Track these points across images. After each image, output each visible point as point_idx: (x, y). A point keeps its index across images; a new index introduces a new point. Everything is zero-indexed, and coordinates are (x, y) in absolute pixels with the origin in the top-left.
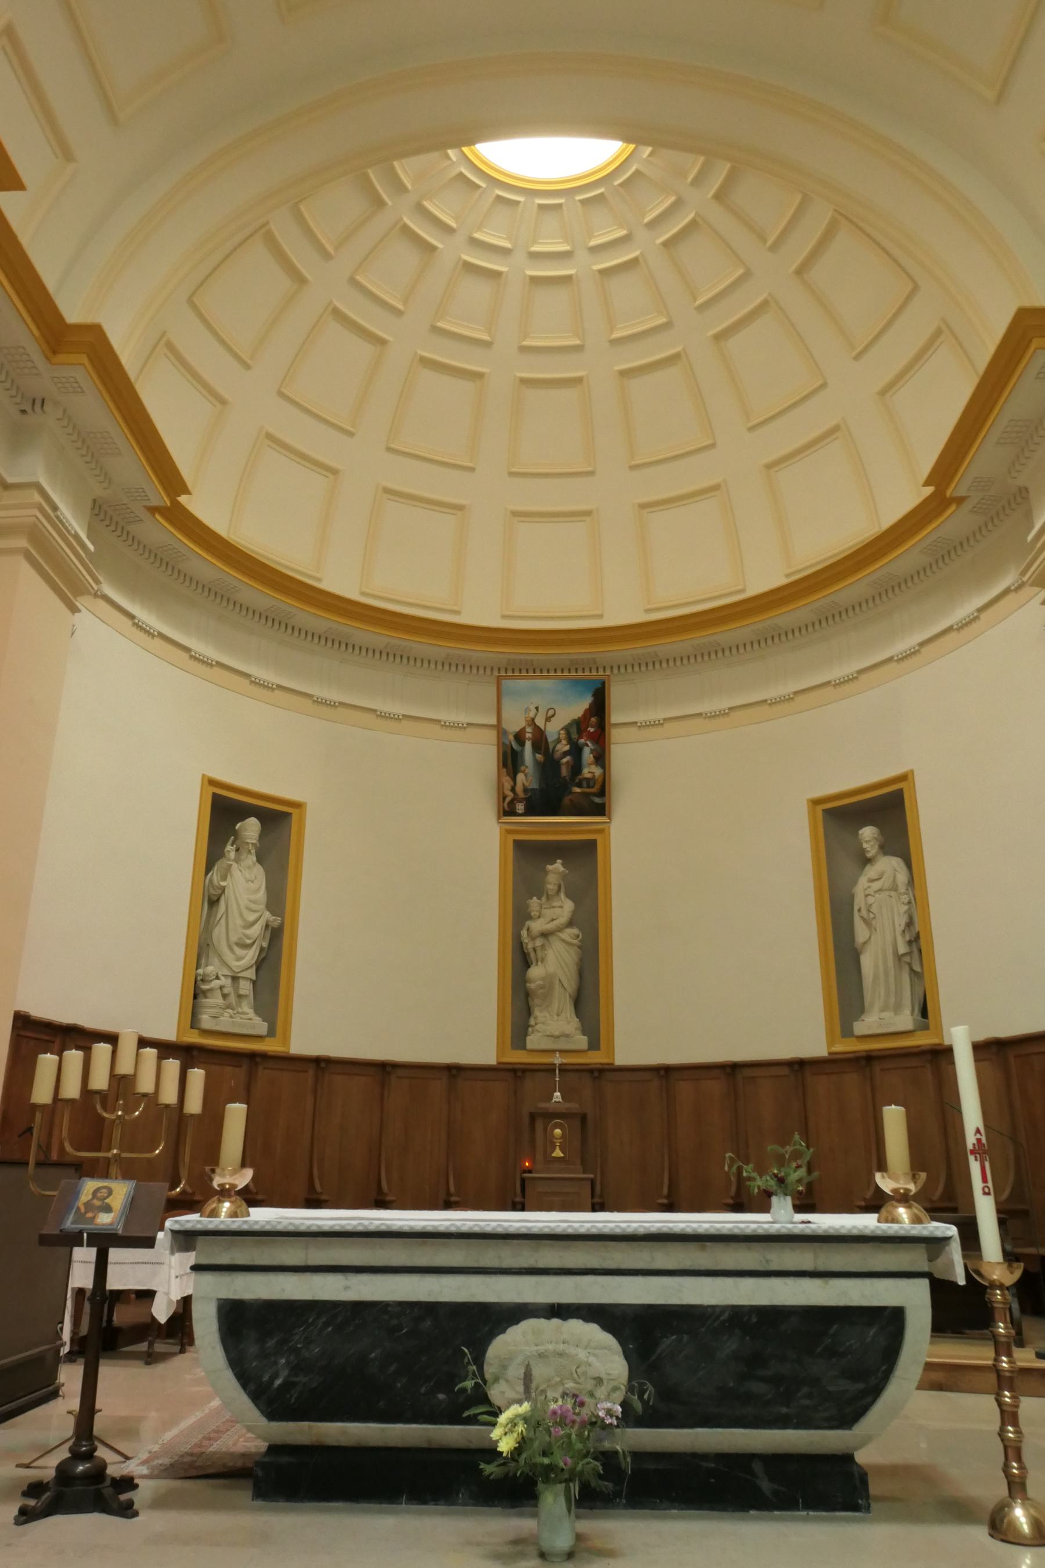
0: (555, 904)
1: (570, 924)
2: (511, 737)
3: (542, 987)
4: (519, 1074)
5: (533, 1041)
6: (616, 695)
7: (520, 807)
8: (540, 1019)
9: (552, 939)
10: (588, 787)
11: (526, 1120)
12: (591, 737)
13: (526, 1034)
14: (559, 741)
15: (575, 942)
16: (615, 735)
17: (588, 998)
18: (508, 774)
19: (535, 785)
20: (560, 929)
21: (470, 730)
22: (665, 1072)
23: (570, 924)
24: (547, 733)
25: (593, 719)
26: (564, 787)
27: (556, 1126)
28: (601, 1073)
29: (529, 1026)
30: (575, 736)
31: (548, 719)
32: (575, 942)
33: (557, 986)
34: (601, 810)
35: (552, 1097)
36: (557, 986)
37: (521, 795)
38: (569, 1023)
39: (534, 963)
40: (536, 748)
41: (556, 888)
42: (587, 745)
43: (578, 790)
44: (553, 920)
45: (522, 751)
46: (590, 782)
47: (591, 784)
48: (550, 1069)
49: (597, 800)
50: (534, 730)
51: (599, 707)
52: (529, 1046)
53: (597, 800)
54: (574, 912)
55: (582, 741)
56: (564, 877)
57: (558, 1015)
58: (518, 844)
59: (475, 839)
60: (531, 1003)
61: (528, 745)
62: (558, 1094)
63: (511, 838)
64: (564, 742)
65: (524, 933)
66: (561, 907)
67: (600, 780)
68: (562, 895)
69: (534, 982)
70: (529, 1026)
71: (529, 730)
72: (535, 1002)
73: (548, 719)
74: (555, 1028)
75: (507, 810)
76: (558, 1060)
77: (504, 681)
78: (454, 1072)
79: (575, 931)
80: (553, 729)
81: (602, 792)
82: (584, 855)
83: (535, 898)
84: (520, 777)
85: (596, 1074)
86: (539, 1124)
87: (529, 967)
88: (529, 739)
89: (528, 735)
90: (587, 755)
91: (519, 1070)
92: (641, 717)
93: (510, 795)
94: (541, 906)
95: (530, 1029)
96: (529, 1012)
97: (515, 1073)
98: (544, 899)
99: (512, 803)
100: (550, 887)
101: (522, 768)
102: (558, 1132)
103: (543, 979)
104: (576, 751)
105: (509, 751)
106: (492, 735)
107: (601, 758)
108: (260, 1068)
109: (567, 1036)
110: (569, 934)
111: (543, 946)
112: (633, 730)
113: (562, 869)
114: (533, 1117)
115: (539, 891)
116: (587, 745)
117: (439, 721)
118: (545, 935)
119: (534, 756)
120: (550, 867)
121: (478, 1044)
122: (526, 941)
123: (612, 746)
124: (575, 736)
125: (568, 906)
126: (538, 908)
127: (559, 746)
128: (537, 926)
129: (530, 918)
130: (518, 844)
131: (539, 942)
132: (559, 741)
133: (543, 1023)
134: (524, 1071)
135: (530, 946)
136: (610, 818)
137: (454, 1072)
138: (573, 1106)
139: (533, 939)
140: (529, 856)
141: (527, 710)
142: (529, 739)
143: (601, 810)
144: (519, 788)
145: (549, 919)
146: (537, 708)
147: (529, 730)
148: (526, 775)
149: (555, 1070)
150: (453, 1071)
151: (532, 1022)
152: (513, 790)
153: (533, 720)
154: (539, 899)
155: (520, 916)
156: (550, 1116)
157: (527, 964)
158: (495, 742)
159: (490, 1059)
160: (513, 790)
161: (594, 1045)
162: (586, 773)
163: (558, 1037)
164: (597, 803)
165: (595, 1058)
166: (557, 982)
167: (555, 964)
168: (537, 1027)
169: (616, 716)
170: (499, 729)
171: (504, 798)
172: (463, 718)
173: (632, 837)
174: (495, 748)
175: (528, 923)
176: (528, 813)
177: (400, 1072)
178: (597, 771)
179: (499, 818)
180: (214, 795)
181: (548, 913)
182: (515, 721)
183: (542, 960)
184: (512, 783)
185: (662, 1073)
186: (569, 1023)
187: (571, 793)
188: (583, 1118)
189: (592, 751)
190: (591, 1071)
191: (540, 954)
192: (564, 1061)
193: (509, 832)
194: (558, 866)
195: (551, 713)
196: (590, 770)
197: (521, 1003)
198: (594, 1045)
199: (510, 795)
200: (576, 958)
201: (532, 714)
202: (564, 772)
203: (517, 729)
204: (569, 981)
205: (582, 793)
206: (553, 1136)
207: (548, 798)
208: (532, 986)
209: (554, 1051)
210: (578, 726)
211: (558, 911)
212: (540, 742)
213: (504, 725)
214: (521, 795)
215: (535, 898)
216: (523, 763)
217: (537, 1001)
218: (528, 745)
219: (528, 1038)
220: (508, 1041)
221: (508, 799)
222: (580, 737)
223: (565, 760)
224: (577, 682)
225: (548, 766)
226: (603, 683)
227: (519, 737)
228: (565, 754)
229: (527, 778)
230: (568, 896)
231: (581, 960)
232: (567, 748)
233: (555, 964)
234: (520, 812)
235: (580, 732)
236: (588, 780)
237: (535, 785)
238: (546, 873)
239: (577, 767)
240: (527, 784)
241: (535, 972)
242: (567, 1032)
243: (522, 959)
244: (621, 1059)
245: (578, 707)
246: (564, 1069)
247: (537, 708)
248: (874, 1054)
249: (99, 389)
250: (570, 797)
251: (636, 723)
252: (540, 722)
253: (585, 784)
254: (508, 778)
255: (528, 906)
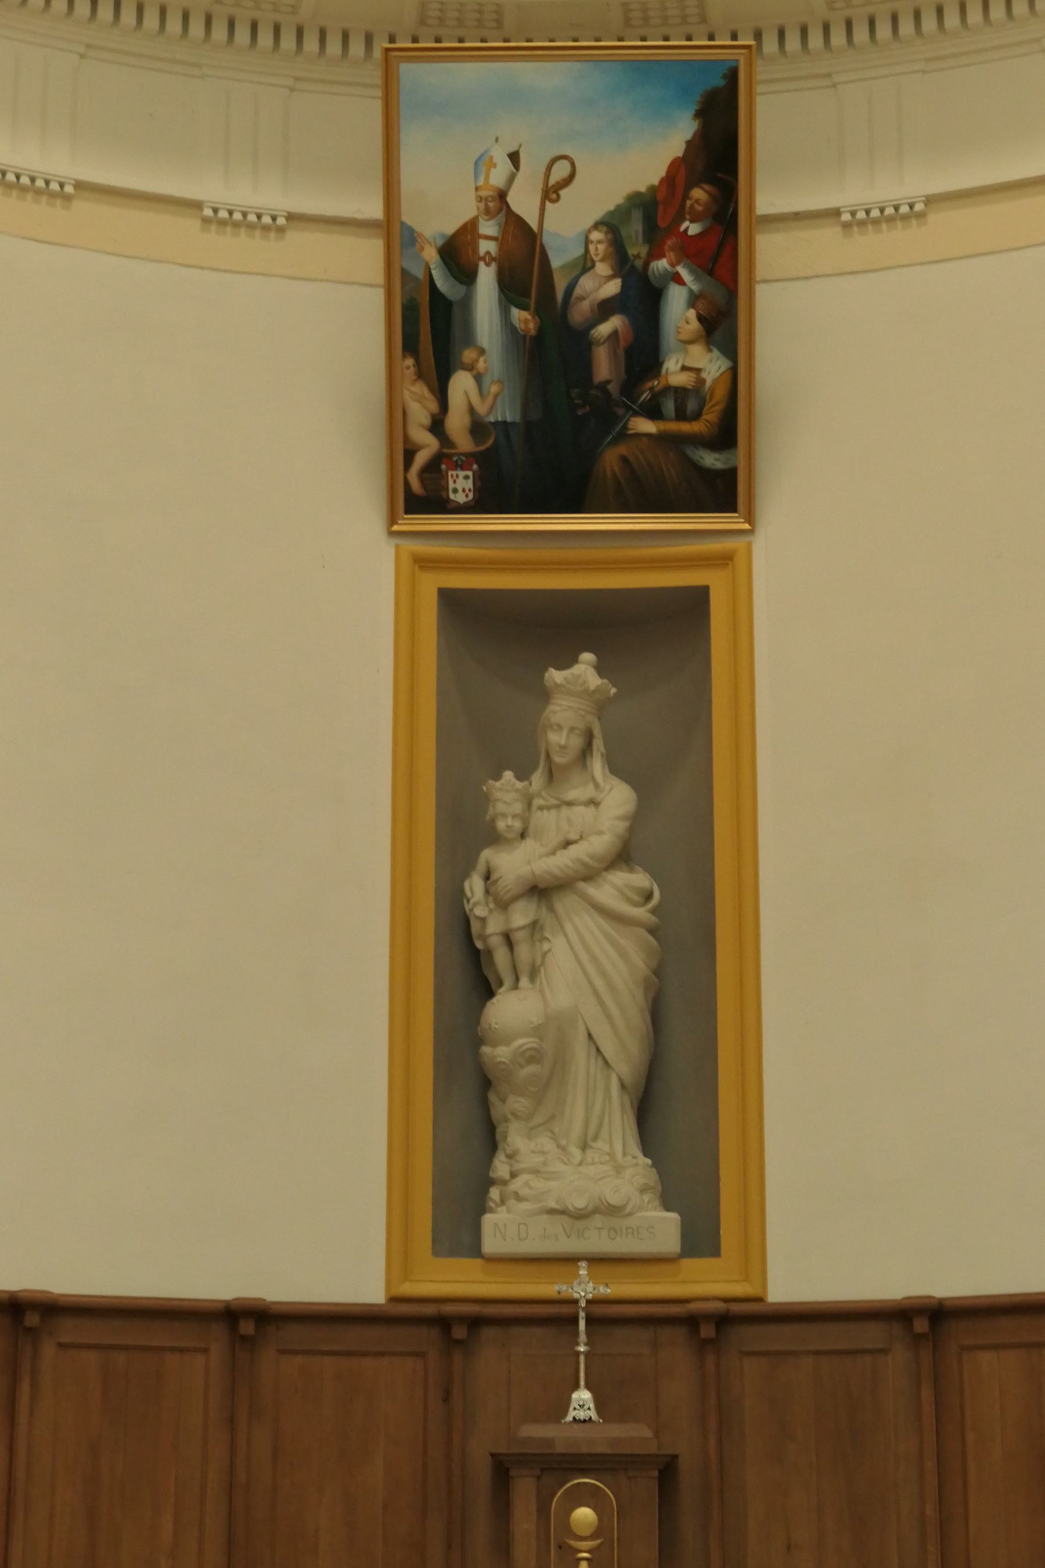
0: (572, 794)
1: (623, 856)
2: (431, 255)
3: (533, 1057)
4: (459, 1332)
5: (503, 1229)
6: (773, 122)
7: (461, 485)
8: (528, 1160)
9: (565, 904)
10: (681, 415)
11: (482, 1472)
12: (690, 251)
13: (481, 1208)
14: (585, 265)
15: (641, 913)
16: (769, 253)
17: (681, 1093)
18: (420, 375)
19: (507, 411)
20: (590, 875)
21: (296, 237)
22: (929, 1323)
23: (623, 856)
24: (546, 239)
25: (699, 194)
26: (605, 415)
27: (577, 1498)
28: (720, 1329)
29: (492, 1182)
30: (637, 249)
31: (551, 193)
32: (641, 913)
33: (580, 1050)
34: (723, 492)
35: (564, 1406)
36: (580, 1050)
37: (464, 443)
38: (619, 1170)
39: (508, 982)
40: (512, 289)
41: (576, 742)
42: (678, 280)
43: (645, 426)
44: (567, 844)
45: (467, 303)
46: (686, 401)
47: (691, 405)
48: (557, 1318)
49: (711, 460)
50: (504, 231)
51: (717, 155)
52: (491, 1244)
53: (711, 460)
54: (637, 820)
55: (662, 264)
56: (602, 706)
57: (584, 1147)
58: (448, 598)
59: (326, 591)
60: (498, 1110)
61: (486, 278)
62: (583, 1395)
63: (431, 584)
64: (603, 269)
65: (475, 886)
66: (593, 803)
67: (721, 393)
68: (597, 766)
69: (507, 1041)
70: (492, 1182)
71: (488, 228)
72: (510, 1105)
73: (551, 193)
74: (575, 1190)
75: (419, 495)
76: (583, 1287)
77: (404, 68)
78: (247, 1328)
79: (640, 879)
80: (569, 227)
81: (726, 435)
82: (665, 636)
83: (508, 775)
84: (461, 384)
85: (707, 1331)
86: (524, 1489)
87: (490, 994)
88: (488, 259)
89: (486, 247)
90: (678, 312)
91: (461, 1319)
92: (852, 193)
93: (428, 445)
94: (529, 802)
95: (494, 1193)
96: (491, 1138)
97: (451, 1330)
98: (538, 779)
99: (434, 468)
100: (556, 738)
101: (468, 355)
102: (584, 1515)
103: (538, 1031)
104: (643, 299)
105: (425, 299)
106: (367, 256)
107: (723, 323)
108: (48, 1351)
109: (612, 1211)
110: (615, 888)
111: (535, 927)
112: (829, 234)
113: (594, 681)
114: (503, 1470)
115: (523, 755)
116: (678, 280)
117: (196, 205)
118: (541, 891)
119: (505, 314)
120: (555, 676)
121: (327, 1239)
122: (480, 911)
123: (760, 290)
124: (637, 249)
125: (618, 799)
126: (518, 807)
127: (586, 283)
128: (513, 864)
129: (494, 838)
130: (451, 601)
131: (521, 916)
132: (585, 265)
133: (536, 1172)
134: (475, 1323)
135: (494, 926)
136: (750, 519)
137: (247, 1328)
138: (634, 1434)
139: (504, 906)
140: (492, 640)
141: (483, 163)
142: (488, 259)
143: (723, 492)
144: (457, 423)
145: (554, 838)
146: (514, 158)
147: (488, 228)
148: (478, 378)
149: (575, 1321)
150: (246, 1324)
151: (501, 1168)
152: (437, 426)
153: (502, 196)
154: (523, 775)
155: (462, 831)
156: (560, 1465)
157: (485, 988)
158: (379, 276)
159: (366, 1286)
160: (437, 426)
161: (701, 1239)
162: (674, 370)
163: (580, 1215)
164: (706, 467)
165: (706, 1282)
166: (582, 1036)
167: (575, 984)
168: (516, 1185)
169: (771, 190)
170: (394, 232)
171: (409, 455)
172: (273, 197)
173: (823, 580)
174: (378, 296)
175: (487, 854)
176: (486, 501)
177: (69, 1330)
178: (712, 365)
179: (392, 520)
180: (448, 598)
181: (549, 823)
182: (442, 199)
183: (534, 974)
184: (434, 406)
185: (921, 1325)
186: (619, 1170)
187: (623, 435)
188: (667, 1470)
189: (693, 301)
190: (692, 1322)
191: (523, 951)
192: (605, 1291)
193: (423, 563)
194: (585, 669)
195: (561, 170)
196: (687, 361)
197: (464, 1109)
198: (701, 1239)
199: (428, 445)
200: (640, 963)
201: (498, 177)
202: (604, 367)
203: (450, 228)
204: (624, 1047)
205: (661, 438)
206: (566, 1527)
207: (545, 459)
208: (498, 1054)
209: (570, 1260)
210: (650, 214)
211: (581, 814)
212: (525, 267)
213: (409, 216)
214: (464, 443)
215: (508, 775)
216: (469, 339)
217: (517, 1103)
218: (486, 278)
219: (488, 1219)
220: (457, 312)
221: (421, 459)
222: (656, 253)
223: (604, 329)
224: (643, 70)
225: (552, 349)
226: (732, 76)
227: (457, 254)
228: (606, 309)
229: (483, 389)
230: (615, 768)
231: (658, 972)
232: (613, 288)
233: (575, 984)
234: (461, 498)
235: (656, 236)
236: (680, 393)
237: (507, 411)
238: (545, 695)
239: (644, 353)
240: (482, 409)
241: (510, 1011)
242: (614, 1200)
243: (470, 971)
244: (786, 1285)
245: (649, 151)
246: (605, 1318)
247: (514, 158)
248: (736, 1308)
249: (596, 992)
250: (622, 449)
251: (836, 213)
252: (524, 203)
253: (669, 406)
254: (421, 389)
255: (486, 799)
